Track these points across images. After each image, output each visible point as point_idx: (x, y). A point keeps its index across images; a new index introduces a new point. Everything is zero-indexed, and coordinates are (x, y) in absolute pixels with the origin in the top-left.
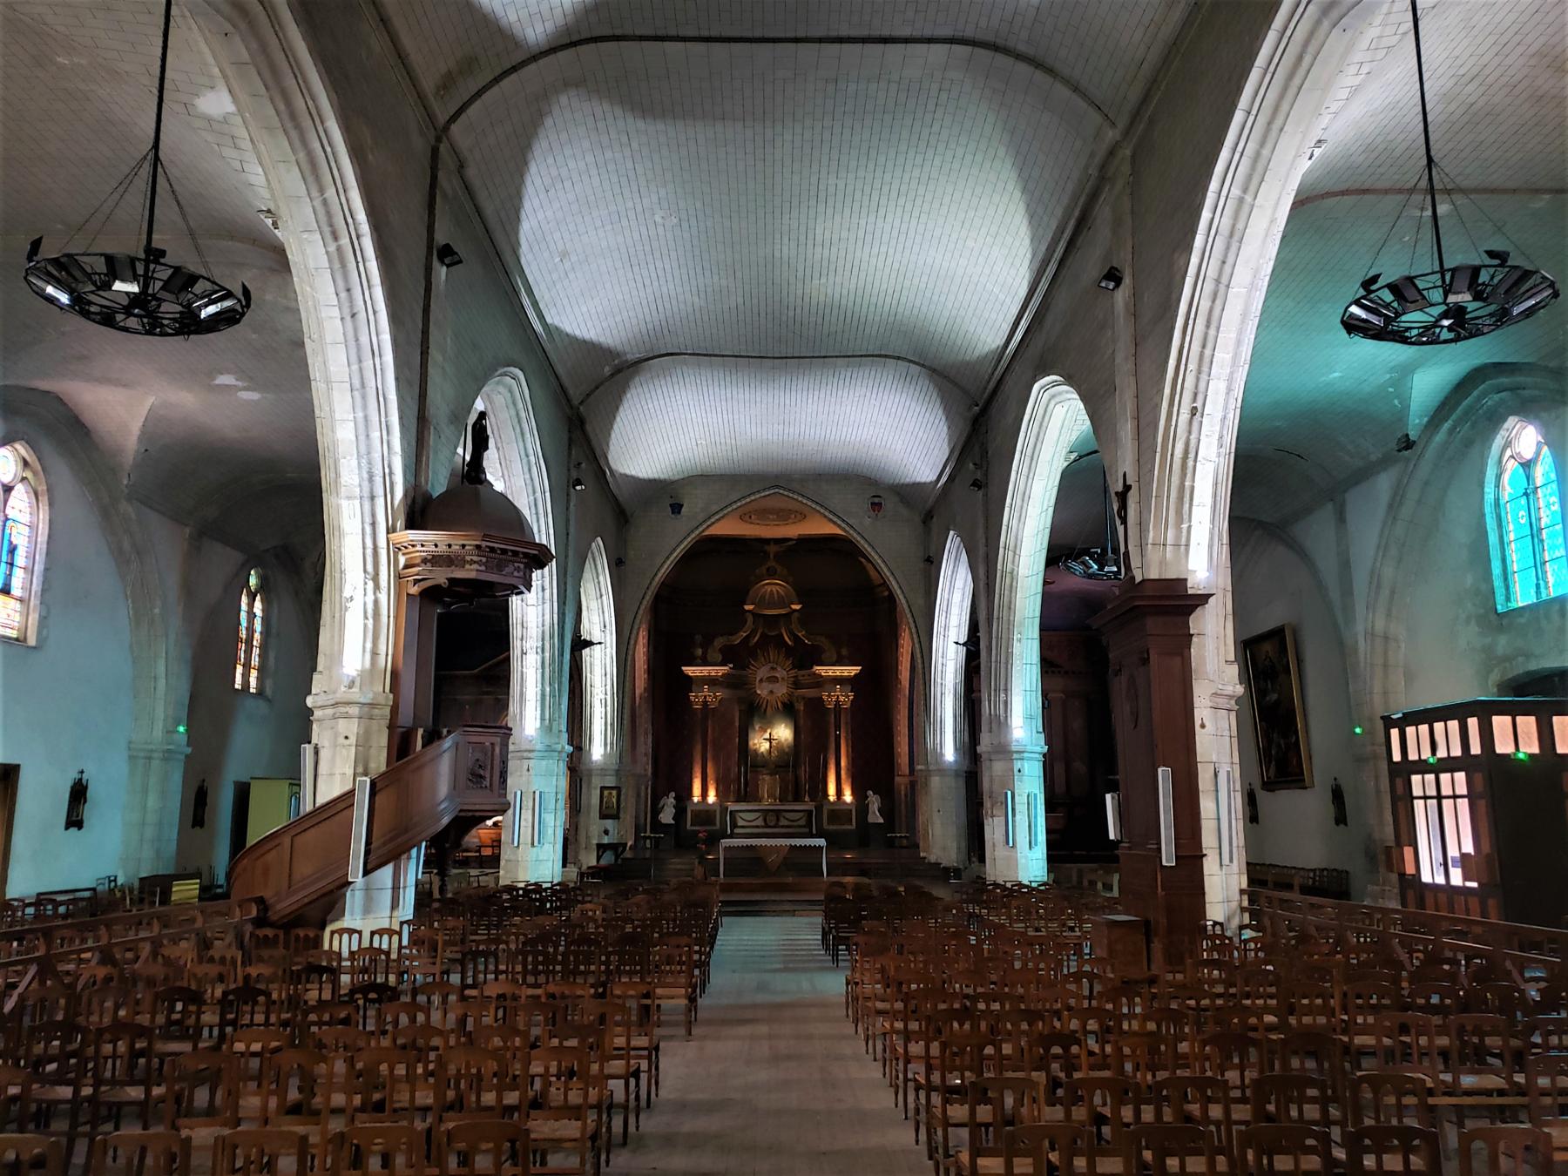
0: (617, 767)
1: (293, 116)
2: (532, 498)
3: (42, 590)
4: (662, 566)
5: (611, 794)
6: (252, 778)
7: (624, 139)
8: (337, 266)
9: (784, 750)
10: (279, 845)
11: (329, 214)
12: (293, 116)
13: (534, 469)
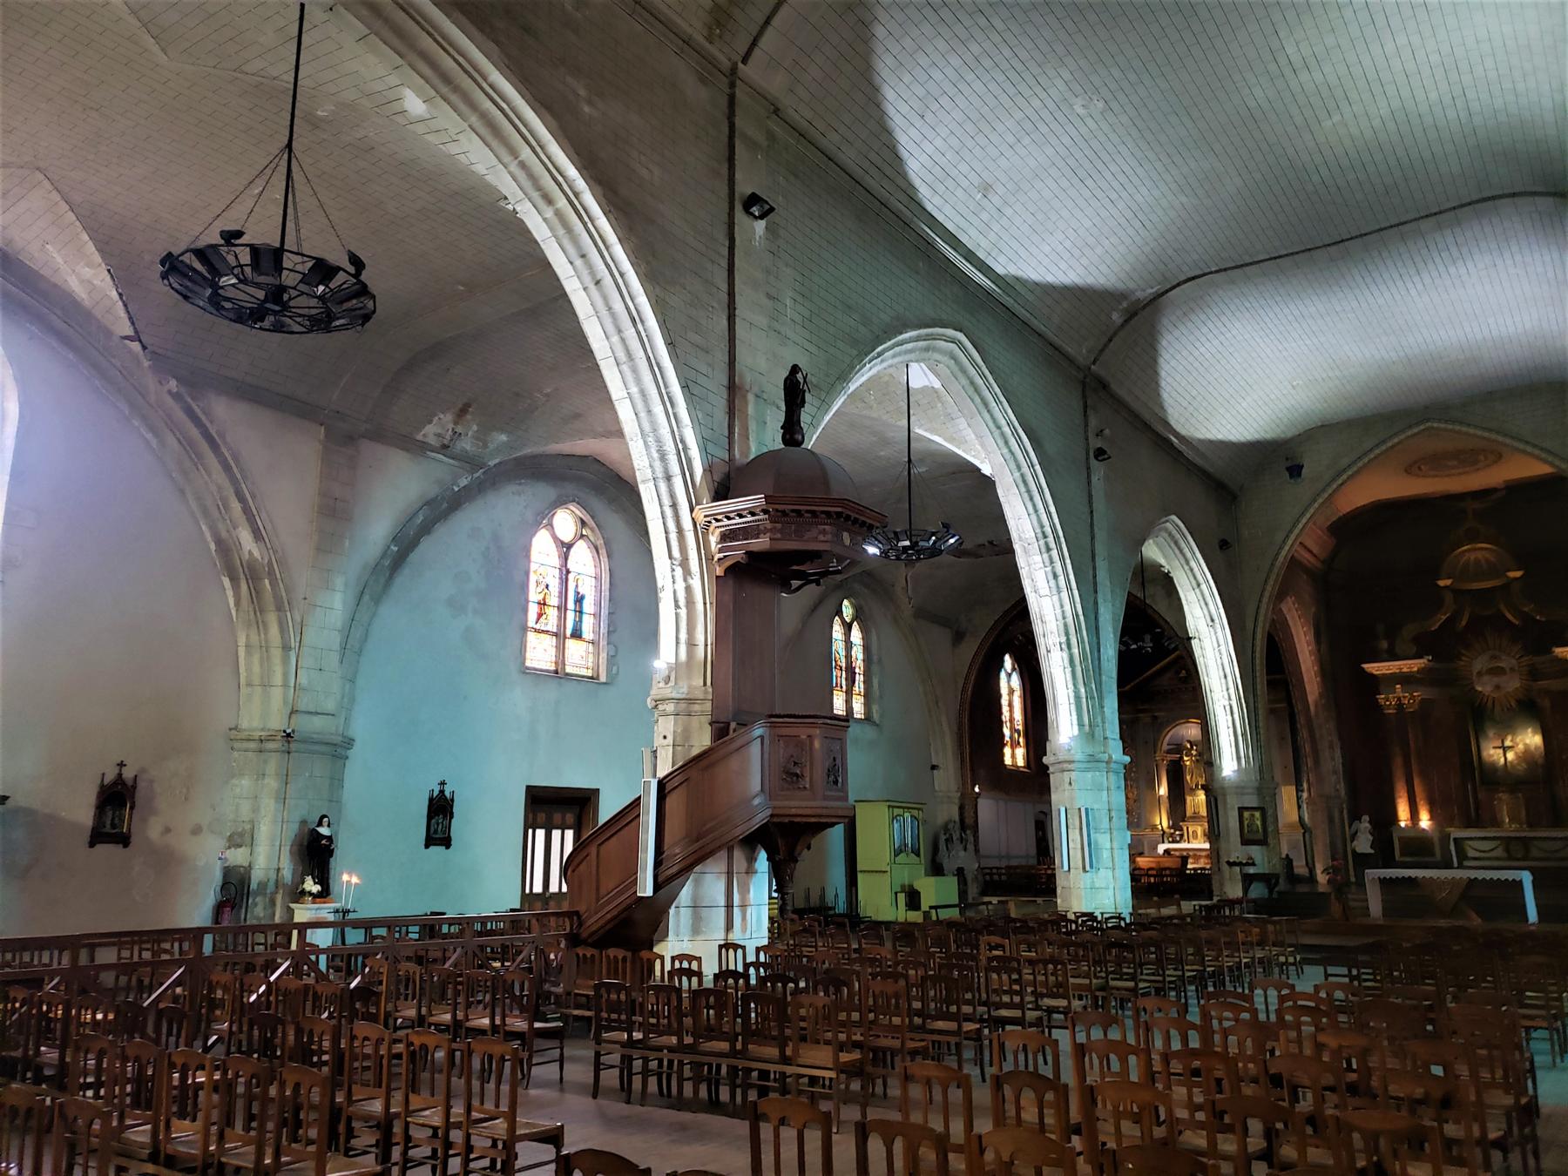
0: (1256, 784)
1: (446, 79)
2: (1017, 474)
3: (608, 632)
4: (1284, 542)
5: (1253, 816)
6: (856, 801)
7: (982, 21)
8: (561, 232)
9: (1536, 763)
10: (587, 856)
11: (532, 177)
12: (446, 79)
13: (1012, 442)
